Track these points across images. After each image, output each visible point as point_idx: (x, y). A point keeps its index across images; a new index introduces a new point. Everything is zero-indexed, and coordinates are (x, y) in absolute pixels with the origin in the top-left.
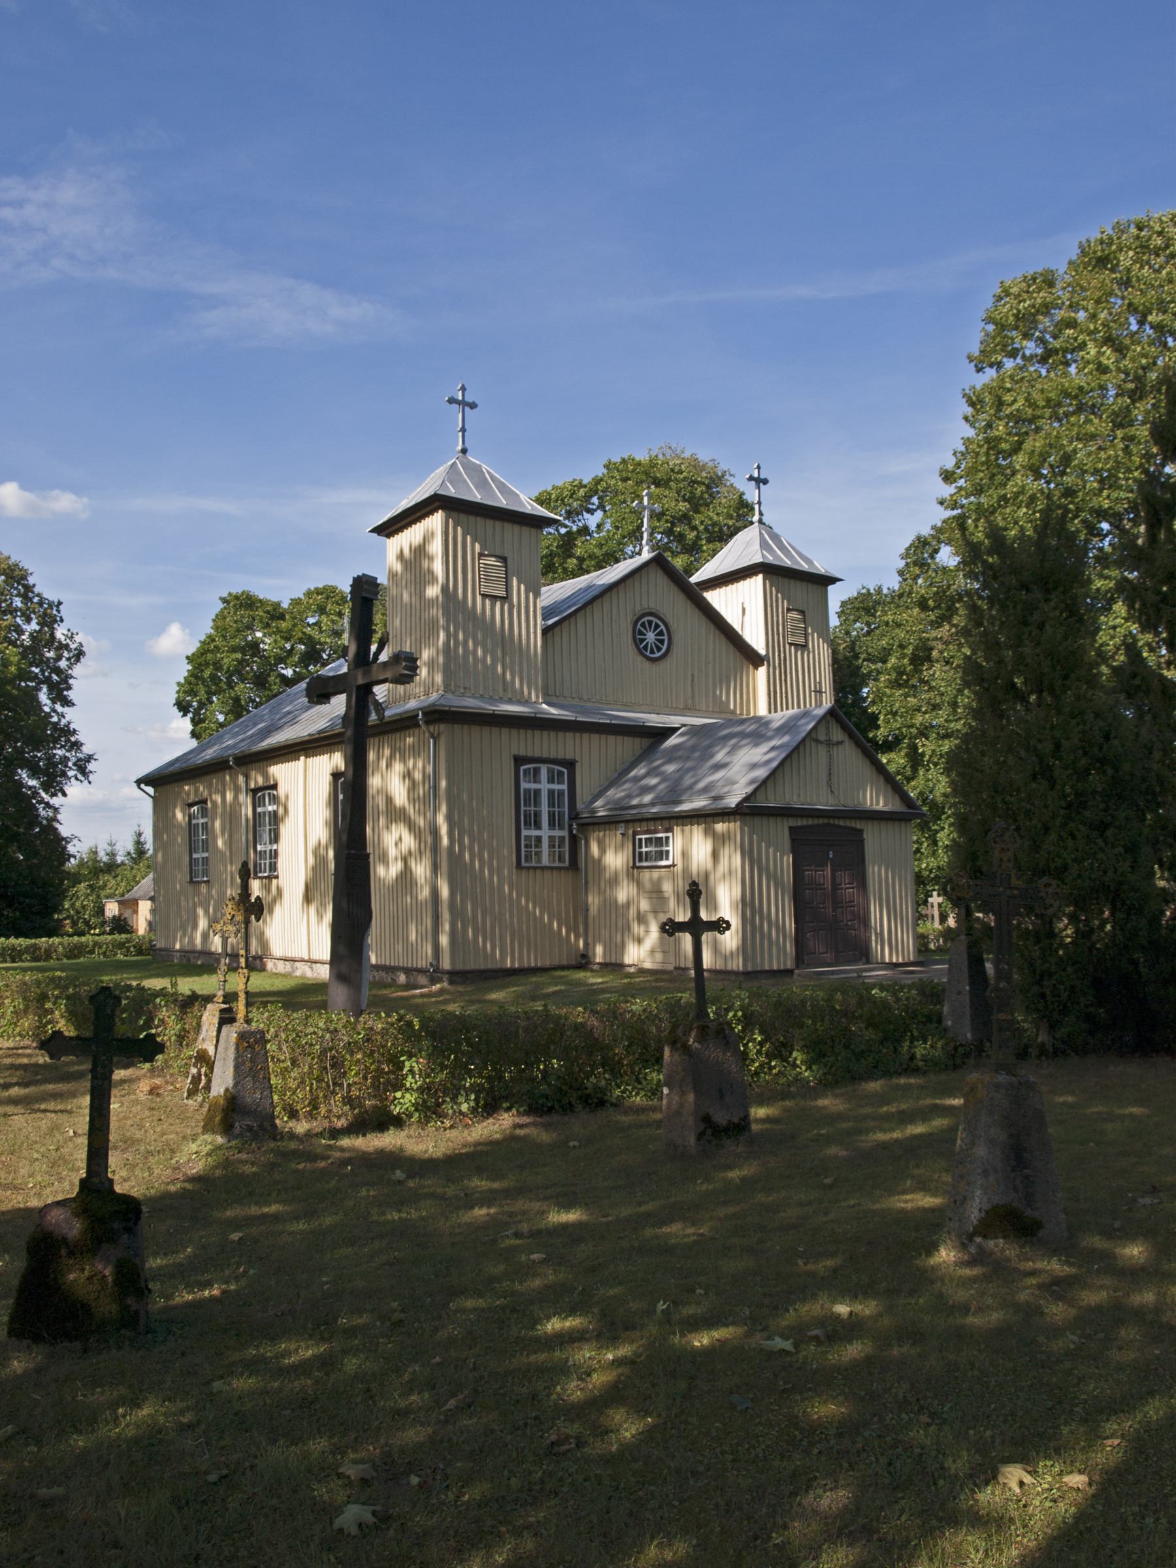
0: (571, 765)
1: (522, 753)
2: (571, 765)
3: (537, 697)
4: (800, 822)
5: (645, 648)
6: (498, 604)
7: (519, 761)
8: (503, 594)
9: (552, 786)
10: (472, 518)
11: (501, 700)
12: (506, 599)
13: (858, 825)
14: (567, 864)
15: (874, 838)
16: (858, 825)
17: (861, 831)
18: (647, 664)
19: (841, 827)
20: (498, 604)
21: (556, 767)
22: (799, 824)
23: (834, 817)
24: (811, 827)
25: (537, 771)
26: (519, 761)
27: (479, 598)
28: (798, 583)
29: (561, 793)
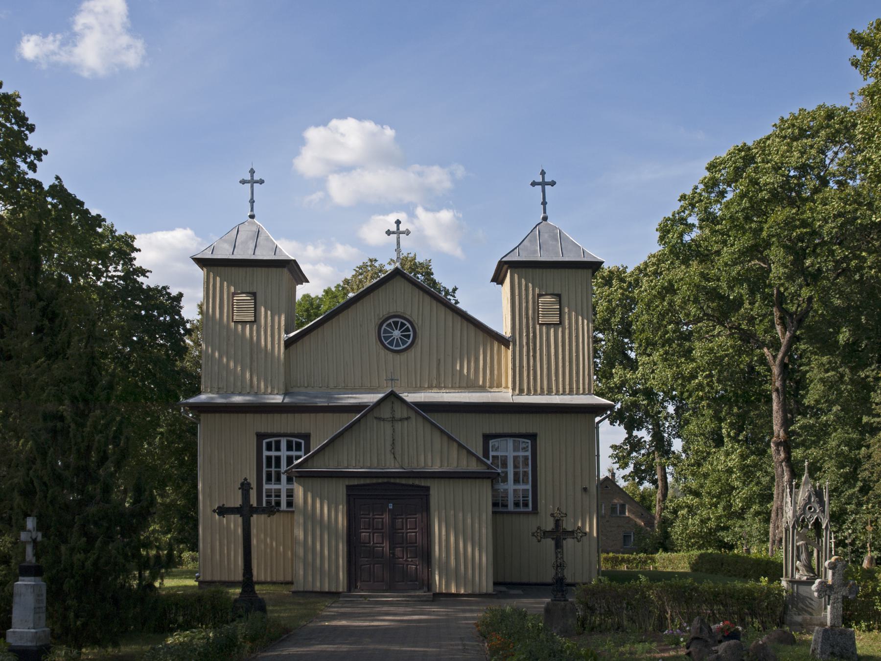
0: (533, 437)
1: (487, 432)
2: (533, 437)
3: (266, 387)
4: (355, 482)
5: (391, 343)
6: (248, 326)
7: (260, 436)
8: (556, 320)
9: (516, 454)
10: (216, 268)
11: (233, 393)
12: (256, 321)
13: (423, 483)
14: (530, 509)
15: (438, 493)
16: (423, 483)
17: (428, 489)
18: (390, 355)
19: (403, 485)
20: (248, 326)
21: (294, 440)
22: (356, 483)
23: (390, 477)
24: (368, 485)
25: (278, 443)
26: (260, 436)
27: (538, 327)
28: (259, 269)
29: (526, 458)
